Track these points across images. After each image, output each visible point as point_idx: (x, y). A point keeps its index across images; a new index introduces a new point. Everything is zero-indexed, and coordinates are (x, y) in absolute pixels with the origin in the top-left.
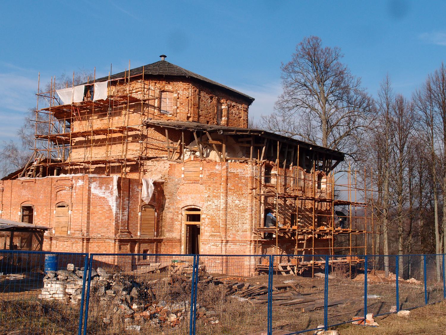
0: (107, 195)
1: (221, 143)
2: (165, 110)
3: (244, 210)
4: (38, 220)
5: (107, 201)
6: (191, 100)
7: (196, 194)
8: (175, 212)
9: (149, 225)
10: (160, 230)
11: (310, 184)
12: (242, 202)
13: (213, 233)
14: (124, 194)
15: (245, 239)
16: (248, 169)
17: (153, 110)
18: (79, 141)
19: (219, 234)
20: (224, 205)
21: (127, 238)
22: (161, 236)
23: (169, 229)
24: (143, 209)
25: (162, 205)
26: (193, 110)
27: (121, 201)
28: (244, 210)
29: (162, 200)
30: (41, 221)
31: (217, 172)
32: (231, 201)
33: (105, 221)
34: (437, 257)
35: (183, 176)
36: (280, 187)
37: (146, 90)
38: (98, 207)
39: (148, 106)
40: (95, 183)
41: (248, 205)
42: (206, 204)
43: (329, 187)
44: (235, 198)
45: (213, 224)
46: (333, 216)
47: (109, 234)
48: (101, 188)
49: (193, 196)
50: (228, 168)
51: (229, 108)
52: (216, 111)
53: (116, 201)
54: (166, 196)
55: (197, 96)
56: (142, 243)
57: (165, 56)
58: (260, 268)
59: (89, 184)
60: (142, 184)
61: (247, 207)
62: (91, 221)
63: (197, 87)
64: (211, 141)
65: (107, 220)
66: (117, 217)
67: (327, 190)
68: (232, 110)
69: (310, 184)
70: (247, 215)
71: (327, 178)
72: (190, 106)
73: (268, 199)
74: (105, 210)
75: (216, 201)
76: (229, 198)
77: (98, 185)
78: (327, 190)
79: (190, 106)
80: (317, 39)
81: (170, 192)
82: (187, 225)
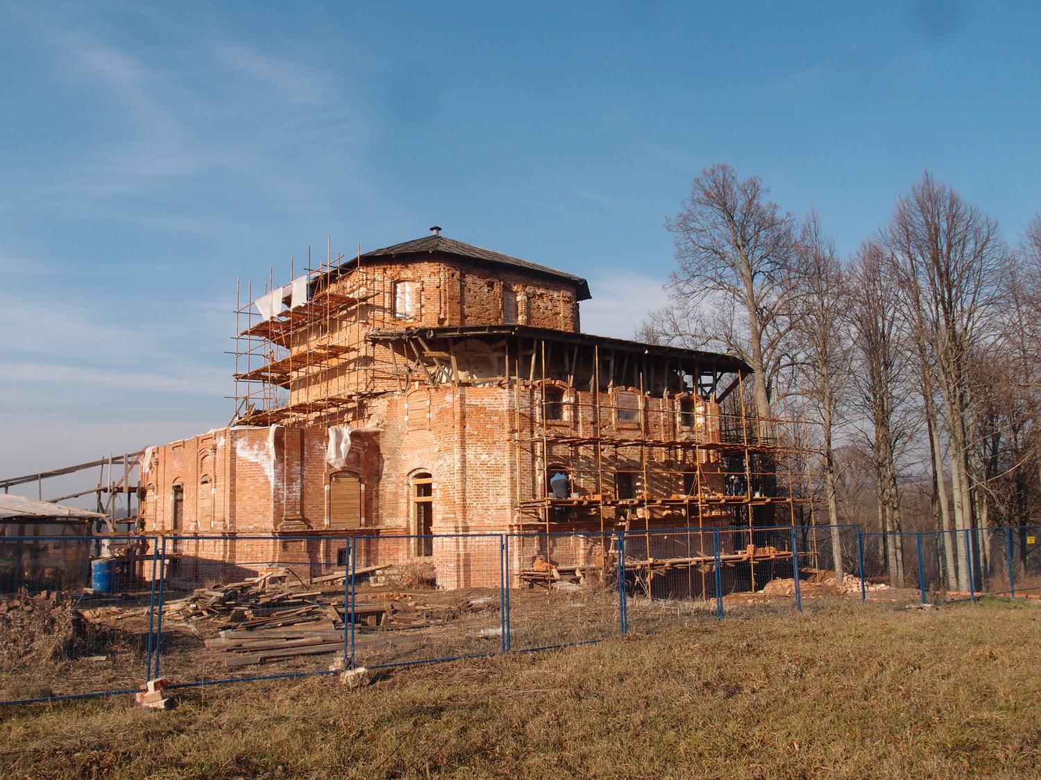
0: (261, 458)
1: (447, 355)
2: (403, 312)
3: (497, 471)
5: (262, 470)
6: (445, 290)
8: (400, 482)
9: (347, 506)
10: (374, 514)
11: (662, 418)
12: (493, 457)
13: (446, 516)
14: (292, 455)
15: (501, 524)
16: (503, 396)
17: (381, 313)
19: (453, 516)
20: (459, 465)
21: (298, 530)
22: (377, 524)
23: (391, 511)
24: (334, 479)
25: (378, 471)
26: (450, 307)
27: (286, 468)
28: (497, 471)
29: (377, 463)
31: (448, 406)
32: (472, 457)
33: (259, 503)
34: (203, 554)
35: (406, 418)
36: (583, 425)
37: (369, 282)
38: (248, 479)
39: (372, 307)
40: (242, 440)
41: (507, 461)
42: (436, 465)
43: (712, 421)
44: (479, 450)
45: (447, 500)
46: (698, 472)
47: (267, 524)
48: (252, 448)
49: (421, 451)
50: (465, 398)
51: (529, 298)
52: (500, 305)
53: (275, 468)
54: (384, 456)
55: (458, 283)
56: (331, 538)
57: (439, 229)
58: (532, 575)
59: (232, 443)
60: (328, 437)
61: (504, 465)
62: (238, 503)
63: (455, 268)
64: (428, 352)
65: (263, 500)
66: (278, 494)
67: (706, 426)
68: (539, 302)
69: (662, 418)
70: (505, 479)
71: (706, 406)
72: (443, 300)
73: (554, 449)
74: (258, 485)
75: (447, 458)
76: (468, 451)
77: (246, 443)
78: (706, 426)
79: (443, 300)
80: (724, 168)
81: (391, 448)
82: (419, 504)
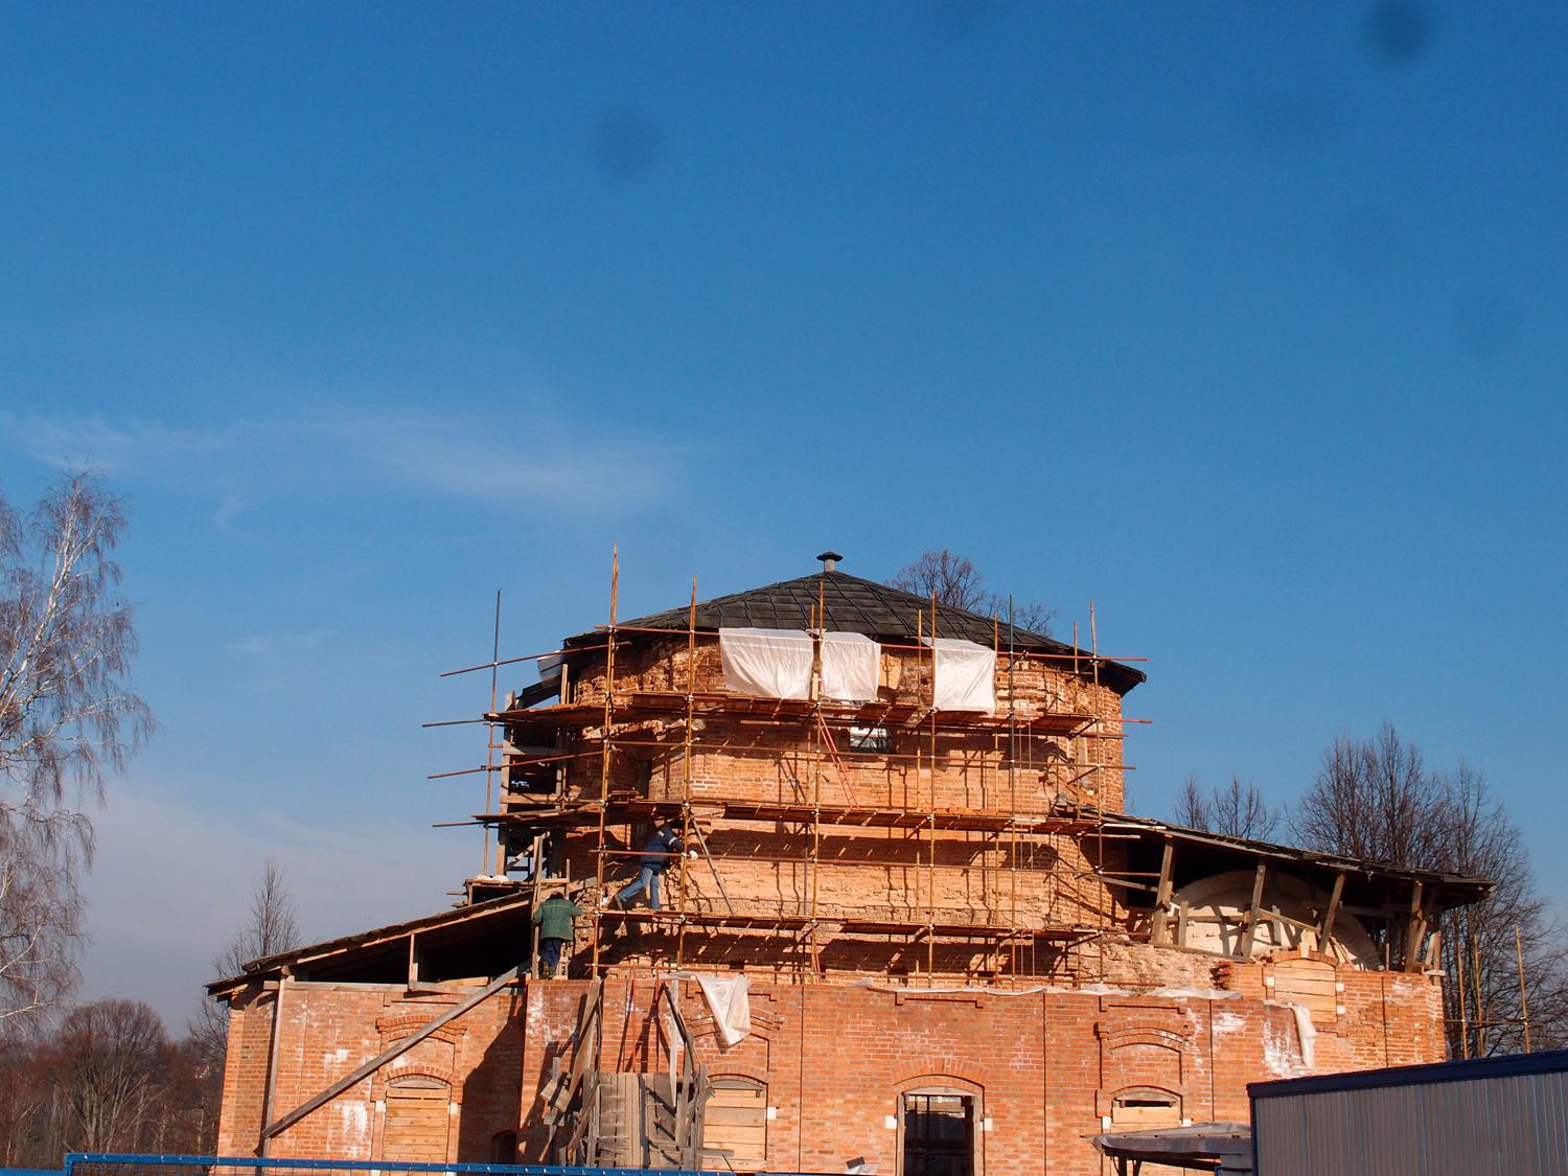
4: (1010, 1151)
7: (1326, 1066)
18: (732, 831)
30: (1025, 1157)
